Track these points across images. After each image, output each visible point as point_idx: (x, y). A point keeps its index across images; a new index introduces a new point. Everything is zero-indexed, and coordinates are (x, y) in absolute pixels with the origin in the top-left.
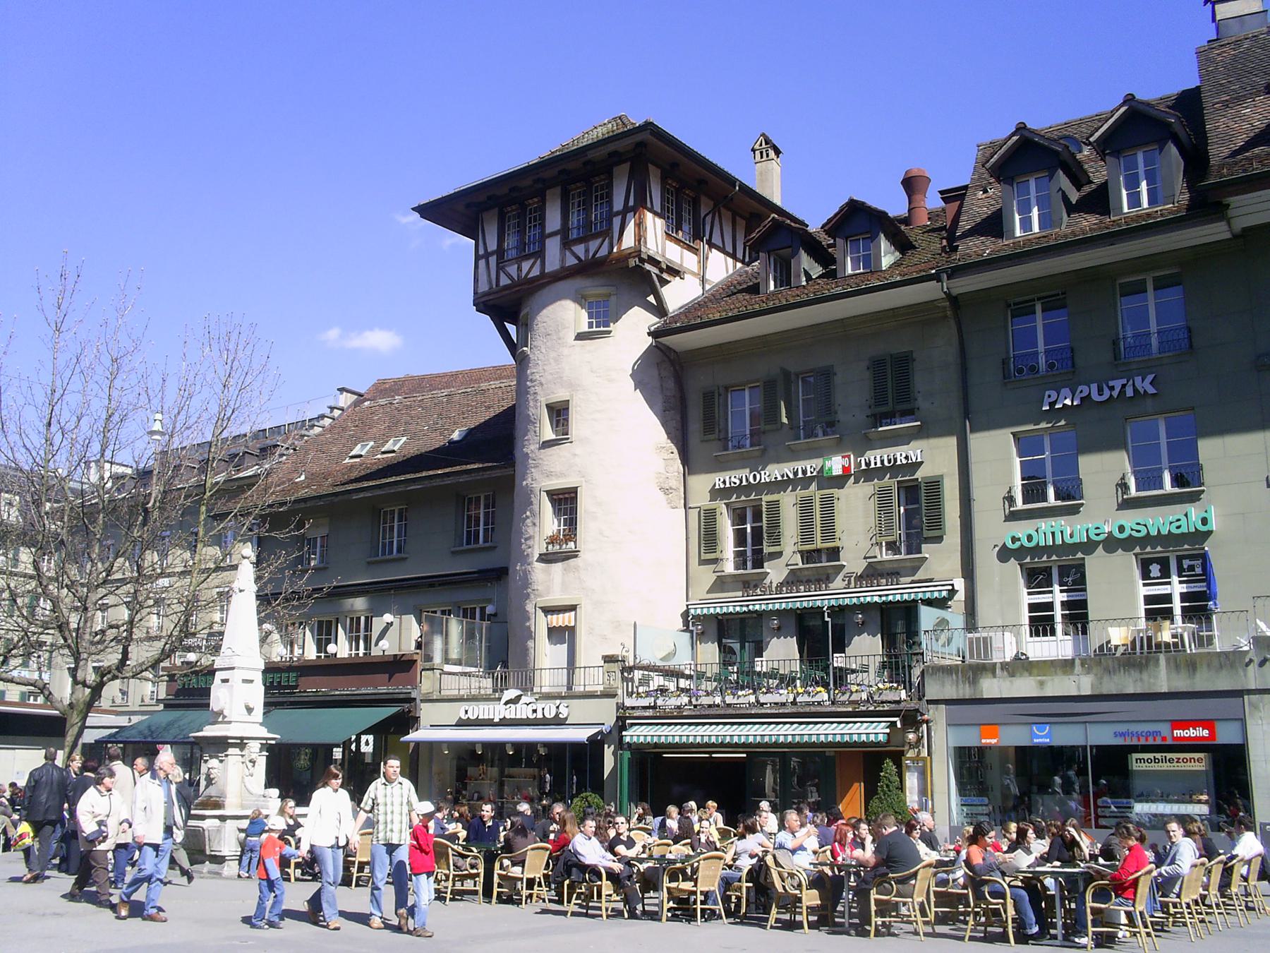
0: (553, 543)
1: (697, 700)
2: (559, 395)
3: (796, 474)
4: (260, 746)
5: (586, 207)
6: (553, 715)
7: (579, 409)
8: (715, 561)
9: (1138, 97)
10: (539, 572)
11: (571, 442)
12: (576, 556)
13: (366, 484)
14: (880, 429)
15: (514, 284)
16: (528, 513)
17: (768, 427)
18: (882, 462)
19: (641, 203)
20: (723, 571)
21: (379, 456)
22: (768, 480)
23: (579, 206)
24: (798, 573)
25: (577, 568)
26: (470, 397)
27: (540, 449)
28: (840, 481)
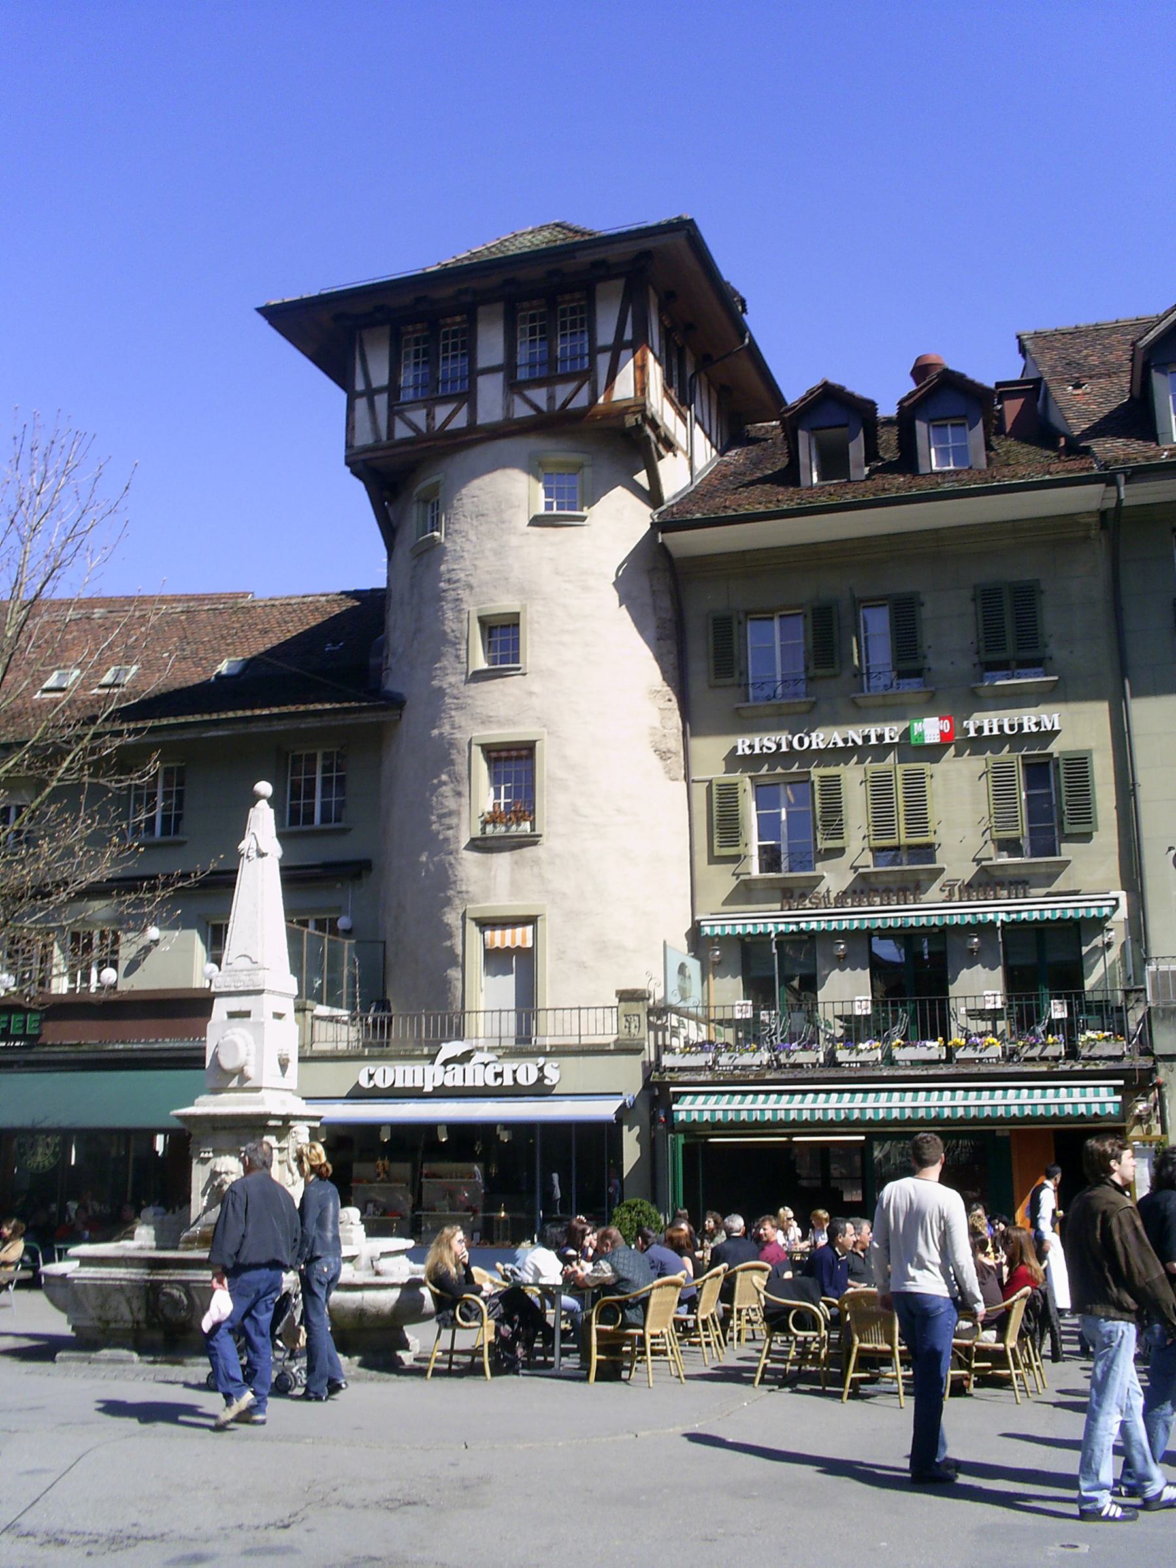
0: (494, 822)
1: (788, 1056)
2: (504, 604)
3: (779, 746)
4: (308, 1130)
5: (546, 333)
6: (533, 1079)
7: (536, 626)
8: (736, 859)
9: (1081, 325)
10: (470, 866)
11: (524, 674)
12: (535, 843)
13: (863, 649)
14: (998, 683)
15: (419, 438)
16: (444, 777)
17: (820, 672)
18: (1001, 728)
19: (639, 342)
20: (749, 873)
21: (95, 691)
22: (822, 746)
23: (417, 357)
24: (873, 879)
25: (536, 862)
26: (226, 616)
27: (467, 682)
28: (933, 753)
